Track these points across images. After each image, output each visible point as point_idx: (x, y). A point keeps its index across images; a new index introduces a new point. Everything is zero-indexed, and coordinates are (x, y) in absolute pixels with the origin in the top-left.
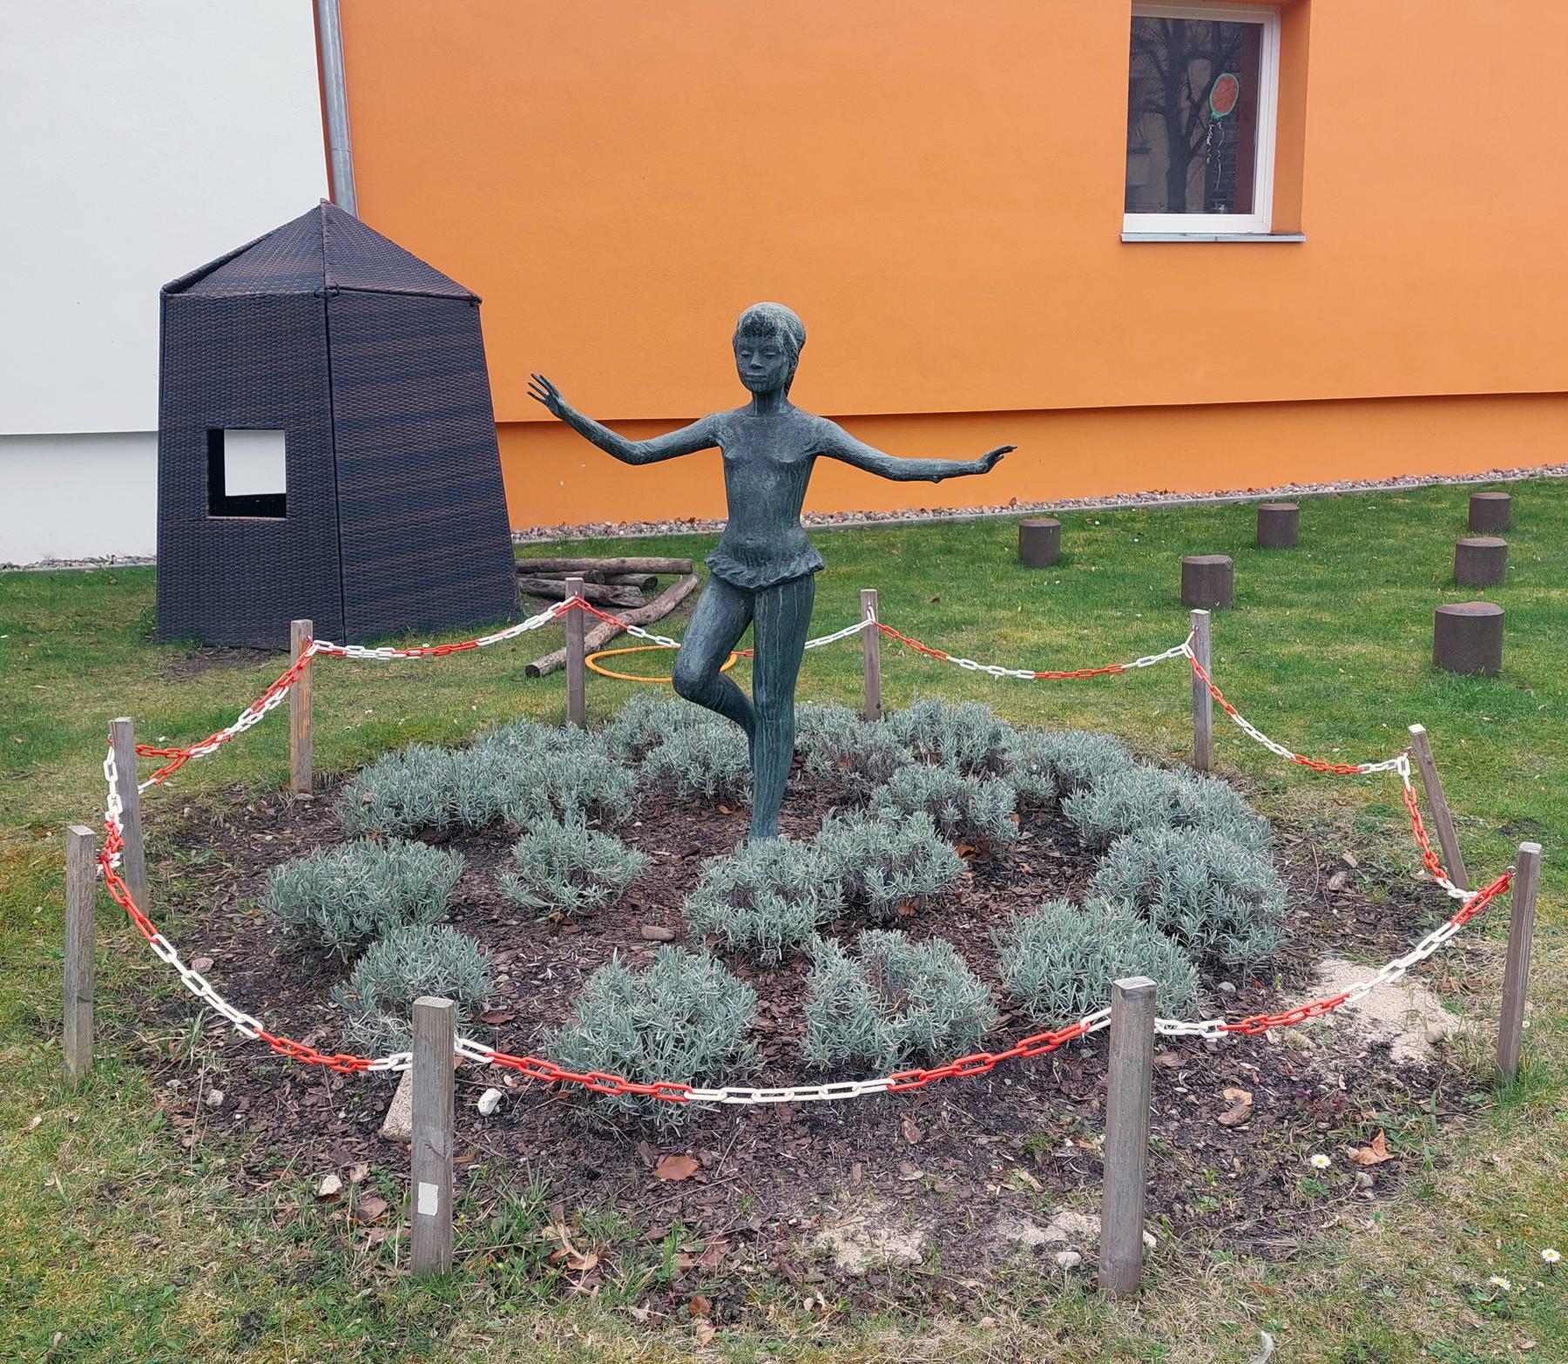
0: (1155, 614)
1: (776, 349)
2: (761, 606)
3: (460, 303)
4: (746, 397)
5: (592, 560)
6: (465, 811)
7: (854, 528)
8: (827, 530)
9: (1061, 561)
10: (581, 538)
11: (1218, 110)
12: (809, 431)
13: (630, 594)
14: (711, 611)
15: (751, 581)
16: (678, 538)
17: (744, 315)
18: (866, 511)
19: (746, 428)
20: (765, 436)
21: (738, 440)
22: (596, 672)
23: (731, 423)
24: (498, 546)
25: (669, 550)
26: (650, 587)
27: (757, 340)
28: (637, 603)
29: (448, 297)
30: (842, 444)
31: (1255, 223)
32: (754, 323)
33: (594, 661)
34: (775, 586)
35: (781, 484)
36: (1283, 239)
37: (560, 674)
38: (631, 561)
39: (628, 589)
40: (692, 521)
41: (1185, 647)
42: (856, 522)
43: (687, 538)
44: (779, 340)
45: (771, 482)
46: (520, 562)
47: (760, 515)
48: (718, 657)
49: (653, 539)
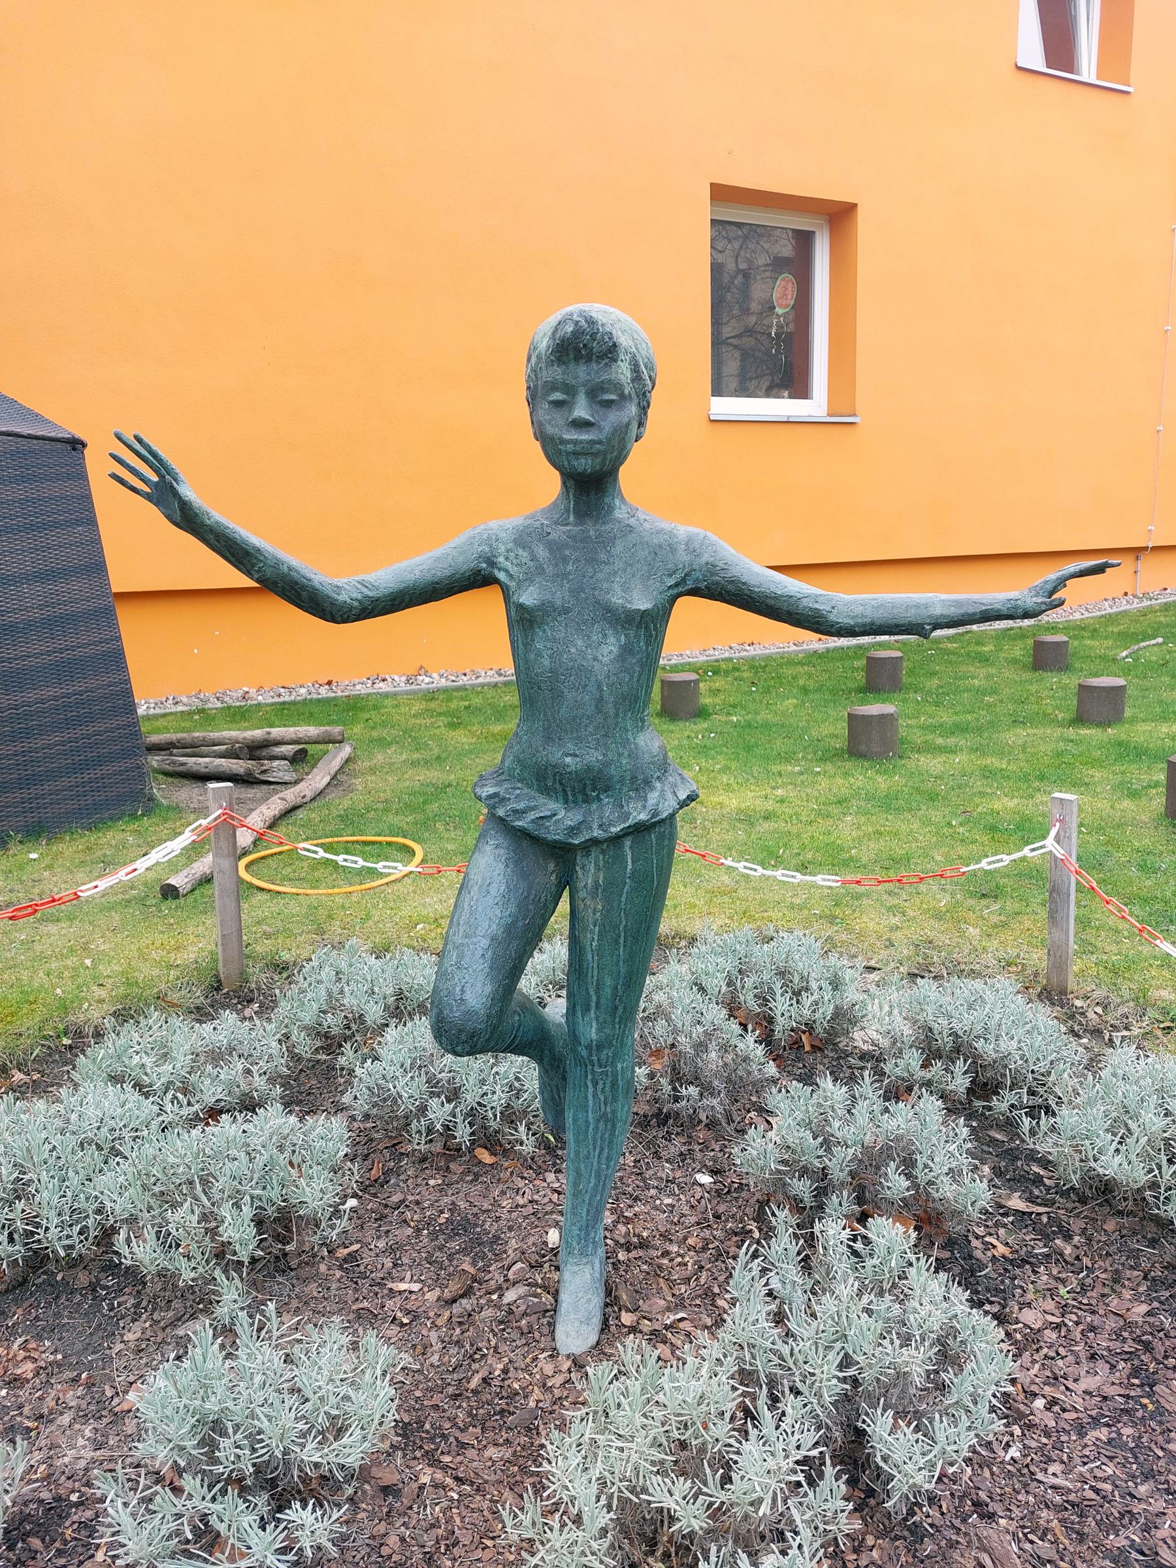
0: (829, 767)
1: (618, 387)
2: (589, 873)
3: (59, 445)
4: (548, 485)
5: (234, 734)
6: (55, 1238)
7: (489, 684)
8: (463, 688)
9: (701, 713)
10: (219, 705)
11: (780, 306)
12: (673, 550)
13: (279, 770)
14: (498, 886)
15: (573, 830)
16: (319, 701)
18: (496, 668)
20: (593, 560)
21: (540, 570)
22: (251, 885)
23: (522, 539)
24: (124, 727)
25: (311, 714)
26: (299, 758)
28: (287, 778)
29: (43, 438)
30: (735, 572)
31: (814, 407)
32: (578, 333)
33: (247, 867)
34: (617, 839)
35: (626, 651)
36: (840, 421)
37: (207, 890)
38: (277, 732)
39: (276, 763)
40: (329, 683)
41: (1050, 843)
42: (488, 680)
43: (326, 701)
44: (623, 371)
45: (609, 648)
46: (154, 739)
47: (590, 710)
48: (511, 967)
49: (294, 703)
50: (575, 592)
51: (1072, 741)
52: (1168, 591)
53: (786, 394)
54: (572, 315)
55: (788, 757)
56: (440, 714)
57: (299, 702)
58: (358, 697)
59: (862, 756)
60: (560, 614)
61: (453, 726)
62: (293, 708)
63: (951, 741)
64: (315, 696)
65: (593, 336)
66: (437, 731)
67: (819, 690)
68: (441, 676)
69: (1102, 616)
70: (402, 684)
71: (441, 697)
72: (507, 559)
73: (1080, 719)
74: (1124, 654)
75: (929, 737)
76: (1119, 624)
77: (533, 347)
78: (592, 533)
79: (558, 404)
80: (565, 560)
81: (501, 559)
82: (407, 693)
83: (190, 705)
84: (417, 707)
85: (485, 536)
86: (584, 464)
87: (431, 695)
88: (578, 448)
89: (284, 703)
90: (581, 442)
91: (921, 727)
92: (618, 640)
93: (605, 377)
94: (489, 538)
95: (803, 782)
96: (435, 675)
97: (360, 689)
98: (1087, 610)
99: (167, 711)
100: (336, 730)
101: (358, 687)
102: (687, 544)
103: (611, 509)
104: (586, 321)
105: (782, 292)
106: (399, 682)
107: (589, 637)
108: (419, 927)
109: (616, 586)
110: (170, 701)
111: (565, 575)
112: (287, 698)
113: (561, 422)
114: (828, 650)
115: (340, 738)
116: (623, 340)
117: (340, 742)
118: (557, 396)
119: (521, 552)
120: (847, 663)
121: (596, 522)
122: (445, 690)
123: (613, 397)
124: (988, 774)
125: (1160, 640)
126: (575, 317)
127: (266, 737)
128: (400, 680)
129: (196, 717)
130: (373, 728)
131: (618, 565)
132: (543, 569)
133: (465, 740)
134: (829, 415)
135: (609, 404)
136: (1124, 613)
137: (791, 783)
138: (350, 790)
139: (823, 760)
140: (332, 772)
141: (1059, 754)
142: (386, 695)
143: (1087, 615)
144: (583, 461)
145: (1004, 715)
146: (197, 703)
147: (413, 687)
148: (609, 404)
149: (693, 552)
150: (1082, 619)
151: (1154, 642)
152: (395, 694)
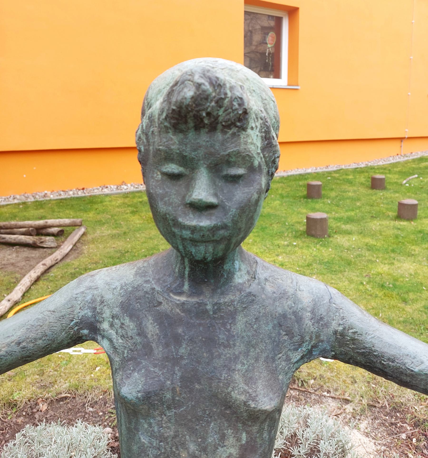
1: (246, 159)
11: (270, 44)
12: (299, 319)
17: (173, 73)
19: (165, 321)
20: (210, 342)
21: (147, 349)
26: (61, 234)
27: (204, 138)
28: (53, 245)
31: (282, 82)
32: (201, 98)
36: (292, 87)
38: (50, 222)
39: (48, 238)
40: (83, 189)
44: (252, 140)
49: (65, 199)
50: (188, 381)
51: (399, 229)
52: (413, 154)
53: (272, 77)
54: (192, 74)
55: (281, 235)
56: (129, 206)
57: (68, 199)
58: (95, 196)
59: (313, 236)
60: (169, 408)
61: (133, 213)
62: (65, 201)
63: (348, 227)
64: (76, 196)
65: (219, 102)
66: (126, 216)
67: (287, 197)
68: (132, 185)
69: (390, 164)
70: (115, 190)
71: (131, 196)
72: (112, 325)
73: (399, 217)
74: (405, 182)
75: (339, 224)
76: (398, 167)
77: (147, 105)
78: (209, 307)
79: (174, 177)
80: (177, 340)
81: (105, 326)
82: (116, 194)
83: (20, 200)
84: (120, 201)
85: (89, 298)
86: (202, 251)
87: (126, 195)
88: (196, 236)
89: (62, 199)
90: (201, 229)
91: (334, 219)
92: (239, 440)
93: (231, 149)
94: (93, 301)
95: (289, 251)
96: (129, 185)
97: (97, 192)
98: (384, 160)
99: (9, 203)
100: (78, 220)
101: (96, 191)
102: (313, 312)
103: (231, 275)
104: (211, 83)
105: (270, 39)
106: (112, 189)
107: (204, 439)
108: (98, 369)
109: (237, 376)
110: (12, 198)
111: (176, 361)
112: (63, 197)
113: (176, 200)
114: (288, 176)
115: (80, 224)
116: (254, 104)
117: (80, 226)
118: (173, 168)
119: (127, 321)
120: (297, 182)
121: (214, 291)
122: (133, 193)
123: (241, 171)
124: (370, 248)
125: (416, 176)
126: (197, 79)
127: (45, 224)
128: (114, 187)
129: (21, 206)
130: (98, 214)
131: (240, 347)
132: (151, 349)
133: (138, 222)
134: (288, 85)
135: (235, 179)
136: (398, 163)
137: (284, 253)
138: (81, 253)
139: (296, 237)
140: (74, 243)
141: (397, 237)
142: (107, 195)
143: (384, 163)
144: (202, 248)
145: (366, 212)
146: (23, 199)
147: (119, 191)
148: (235, 179)
149: (318, 319)
150: (383, 165)
151: (414, 176)
152: (111, 194)
